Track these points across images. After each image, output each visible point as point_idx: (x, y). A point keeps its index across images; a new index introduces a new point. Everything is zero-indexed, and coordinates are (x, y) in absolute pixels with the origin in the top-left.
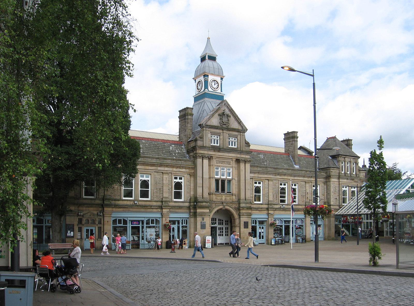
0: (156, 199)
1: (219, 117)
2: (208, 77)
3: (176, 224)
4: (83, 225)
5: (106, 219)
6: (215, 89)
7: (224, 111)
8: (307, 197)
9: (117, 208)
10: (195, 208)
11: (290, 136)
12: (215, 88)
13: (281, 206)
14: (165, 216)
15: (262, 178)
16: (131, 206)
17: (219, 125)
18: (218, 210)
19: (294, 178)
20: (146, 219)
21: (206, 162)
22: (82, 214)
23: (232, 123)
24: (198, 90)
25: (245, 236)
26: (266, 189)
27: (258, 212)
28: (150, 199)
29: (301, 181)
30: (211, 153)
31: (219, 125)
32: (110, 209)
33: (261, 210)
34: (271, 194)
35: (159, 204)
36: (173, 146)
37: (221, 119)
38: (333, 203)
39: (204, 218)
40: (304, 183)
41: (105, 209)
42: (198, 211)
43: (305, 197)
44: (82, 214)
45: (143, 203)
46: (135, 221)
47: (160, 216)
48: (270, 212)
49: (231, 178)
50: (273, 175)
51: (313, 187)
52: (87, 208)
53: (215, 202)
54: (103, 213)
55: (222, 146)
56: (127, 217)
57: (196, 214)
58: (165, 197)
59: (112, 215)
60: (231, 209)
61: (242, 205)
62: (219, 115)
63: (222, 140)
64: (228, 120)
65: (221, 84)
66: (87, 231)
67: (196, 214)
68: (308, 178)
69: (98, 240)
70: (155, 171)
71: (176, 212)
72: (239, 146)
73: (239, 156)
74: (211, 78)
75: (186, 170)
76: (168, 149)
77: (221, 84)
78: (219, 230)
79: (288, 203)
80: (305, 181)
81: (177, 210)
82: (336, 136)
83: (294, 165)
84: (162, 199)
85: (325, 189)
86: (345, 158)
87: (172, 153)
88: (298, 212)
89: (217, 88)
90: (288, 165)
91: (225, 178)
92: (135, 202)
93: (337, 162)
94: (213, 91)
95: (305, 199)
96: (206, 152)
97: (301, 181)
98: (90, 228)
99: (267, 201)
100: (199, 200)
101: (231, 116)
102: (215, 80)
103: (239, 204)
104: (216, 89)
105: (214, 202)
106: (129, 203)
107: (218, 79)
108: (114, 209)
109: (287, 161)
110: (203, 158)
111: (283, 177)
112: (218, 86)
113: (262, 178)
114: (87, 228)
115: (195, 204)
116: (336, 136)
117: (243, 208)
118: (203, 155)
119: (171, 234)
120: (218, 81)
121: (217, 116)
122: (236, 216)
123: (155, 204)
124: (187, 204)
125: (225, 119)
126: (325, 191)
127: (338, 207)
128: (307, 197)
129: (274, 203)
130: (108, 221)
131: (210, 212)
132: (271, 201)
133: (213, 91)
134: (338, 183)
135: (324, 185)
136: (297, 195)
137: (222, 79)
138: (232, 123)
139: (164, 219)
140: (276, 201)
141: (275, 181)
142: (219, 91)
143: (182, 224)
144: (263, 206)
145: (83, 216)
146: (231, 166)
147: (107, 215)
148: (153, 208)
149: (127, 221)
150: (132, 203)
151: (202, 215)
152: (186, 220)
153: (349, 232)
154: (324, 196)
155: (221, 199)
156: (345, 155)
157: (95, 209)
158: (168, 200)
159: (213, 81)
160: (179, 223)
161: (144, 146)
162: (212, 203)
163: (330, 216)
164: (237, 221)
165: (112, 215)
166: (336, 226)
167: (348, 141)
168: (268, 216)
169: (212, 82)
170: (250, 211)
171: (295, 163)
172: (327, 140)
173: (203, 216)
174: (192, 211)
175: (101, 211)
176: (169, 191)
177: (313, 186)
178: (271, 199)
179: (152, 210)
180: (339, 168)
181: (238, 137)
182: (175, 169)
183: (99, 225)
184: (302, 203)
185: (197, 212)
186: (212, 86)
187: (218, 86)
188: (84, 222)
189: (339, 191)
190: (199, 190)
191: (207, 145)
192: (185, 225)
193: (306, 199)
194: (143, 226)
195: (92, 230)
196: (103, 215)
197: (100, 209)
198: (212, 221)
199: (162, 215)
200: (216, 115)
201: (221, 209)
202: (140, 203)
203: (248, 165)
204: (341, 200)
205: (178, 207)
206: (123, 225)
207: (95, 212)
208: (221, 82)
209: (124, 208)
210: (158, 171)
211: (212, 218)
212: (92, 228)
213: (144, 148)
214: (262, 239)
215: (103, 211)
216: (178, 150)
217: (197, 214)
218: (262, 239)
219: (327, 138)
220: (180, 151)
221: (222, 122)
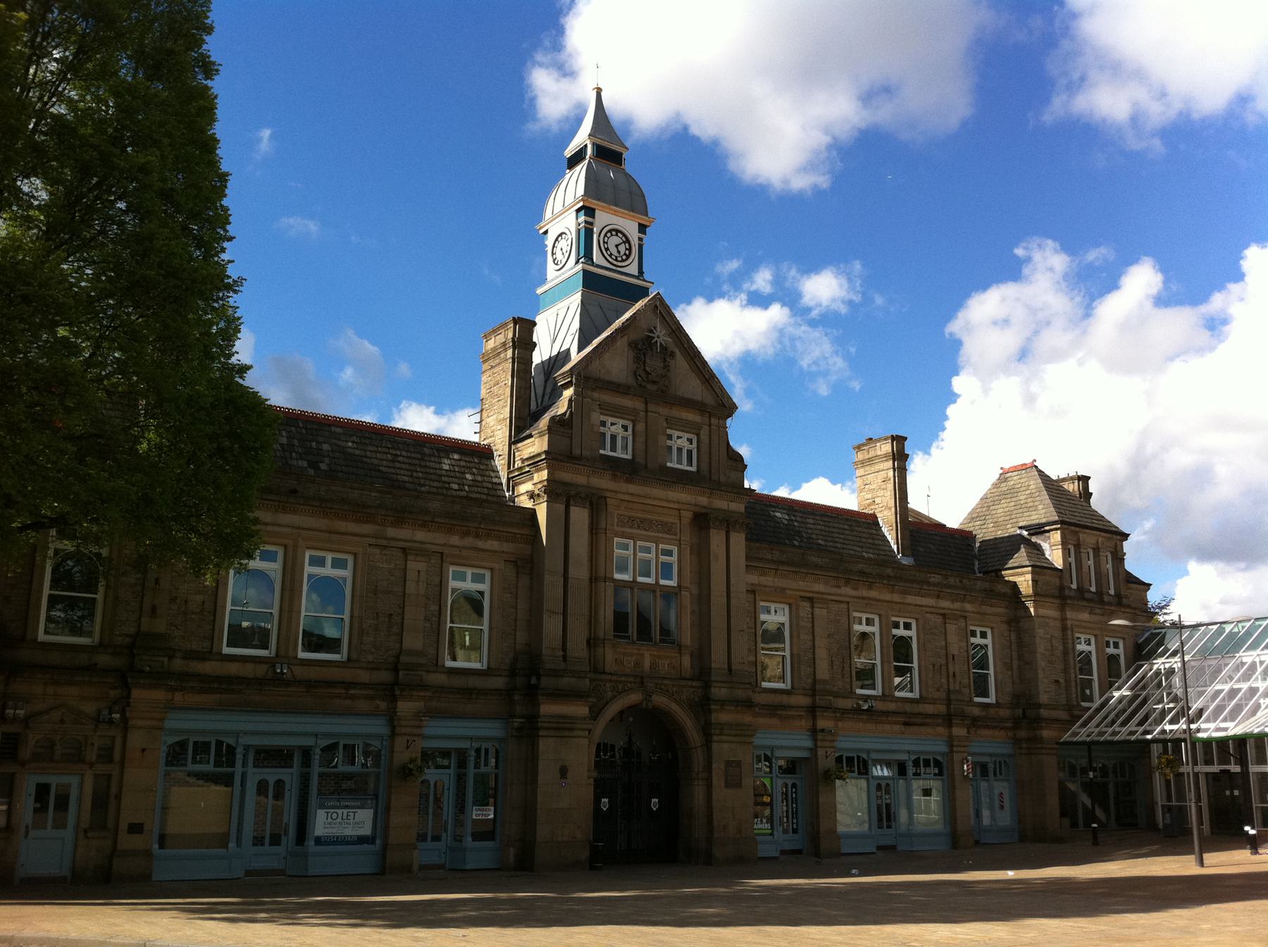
0: (370, 658)
2: (594, 218)
3: (295, 766)
4: (23, 764)
5: (136, 740)
6: (616, 260)
7: (652, 331)
8: (951, 674)
10: (532, 693)
11: (879, 453)
12: (619, 259)
13: (861, 702)
14: (403, 730)
16: (260, 682)
17: (631, 381)
18: (621, 712)
20: (324, 743)
22: (21, 712)
24: (557, 264)
26: (805, 637)
27: (774, 721)
28: (917, 696)
29: (927, 609)
30: (602, 482)
31: (631, 381)
32: (159, 695)
34: (821, 654)
35: (386, 676)
36: (456, 456)
38: (1046, 696)
40: (939, 620)
41: (136, 693)
42: (548, 709)
43: (944, 672)
44: (21, 712)
45: (313, 673)
48: (821, 724)
49: (672, 583)
51: (972, 636)
53: (614, 678)
54: (123, 712)
55: (640, 460)
56: (237, 734)
57: (537, 722)
60: (675, 708)
61: (719, 692)
63: (641, 439)
64: (666, 367)
65: (641, 247)
66: (42, 790)
67: (537, 722)
68: (953, 601)
69: (87, 838)
70: (372, 541)
72: (705, 466)
73: (703, 500)
76: (437, 466)
77: (641, 247)
80: (942, 611)
84: (398, 657)
85: (1014, 647)
87: (449, 483)
88: (923, 729)
89: (624, 257)
90: (877, 552)
91: (654, 582)
92: (278, 666)
93: (1051, 546)
94: (614, 268)
95: (944, 681)
97: (927, 609)
99: (810, 681)
101: (677, 351)
102: (618, 231)
103: (707, 685)
104: (623, 261)
105: (609, 677)
106: (248, 670)
107: (631, 228)
108: (178, 697)
109: (870, 541)
112: (627, 252)
114: (44, 779)
115: (534, 681)
116: (1035, 461)
117: (723, 703)
120: (627, 234)
121: (626, 349)
122: (694, 736)
123: (364, 676)
124: (499, 682)
125: (654, 364)
126: (1015, 654)
127: (1063, 715)
128: (951, 674)
130: (144, 750)
131: (595, 714)
132: (824, 681)
134: (1058, 624)
135: (1010, 631)
137: (642, 228)
139: (400, 742)
141: (835, 607)
142: (633, 269)
143: (477, 766)
145: (26, 722)
146: (676, 540)
147: (140, 723)
148: (353, 698)
149: (235, 749)
150: (261, 670)
151: (564, 726)
153: (1106, 810)
154: (1010, 672)
155: (637, 664)
158: (422, 660)
159: (610, 231)
160: (462, 764)
162: (602, 680)
163: (1039, 746)
164: (698, 758)
165: (168, 724)
166: (1062, 789)
168: (815, 740)
169: (609, 235)
170: (747, 719)
172: (1001, 474)
174: (519, 709)
175: (115, 703)
176: (428, 625)
177: (969, 635)
178: (823, 672)
179: (348, 702)
181: (702, 432)
184: (937, 695)
185: (538, 716)
186: (607, 249)
187: (630, 249)
189: (1065, 653)
190: (551, 626)
191: (586, 453)
193: (951, 680)
194: (465, 775)
195: (280, 784)
196: (125, 720)
197: (113, 693)
198: (598, 755)
199: (393, 728)
201: (632, 708)
202: (299, 672)
203: (739, 541)
204: (1074, 690)
206: (215, 766)
207: (89, 708)
208: (640, 239)
210: (384, 542)
211: (599, 745)
212: (65, 780)
213: (337, 455)
215: (124, 702)
216: (473, 474)
217: (540, 724)
219: (1002, 469)
220: (479, 478)
221: (641, 372)
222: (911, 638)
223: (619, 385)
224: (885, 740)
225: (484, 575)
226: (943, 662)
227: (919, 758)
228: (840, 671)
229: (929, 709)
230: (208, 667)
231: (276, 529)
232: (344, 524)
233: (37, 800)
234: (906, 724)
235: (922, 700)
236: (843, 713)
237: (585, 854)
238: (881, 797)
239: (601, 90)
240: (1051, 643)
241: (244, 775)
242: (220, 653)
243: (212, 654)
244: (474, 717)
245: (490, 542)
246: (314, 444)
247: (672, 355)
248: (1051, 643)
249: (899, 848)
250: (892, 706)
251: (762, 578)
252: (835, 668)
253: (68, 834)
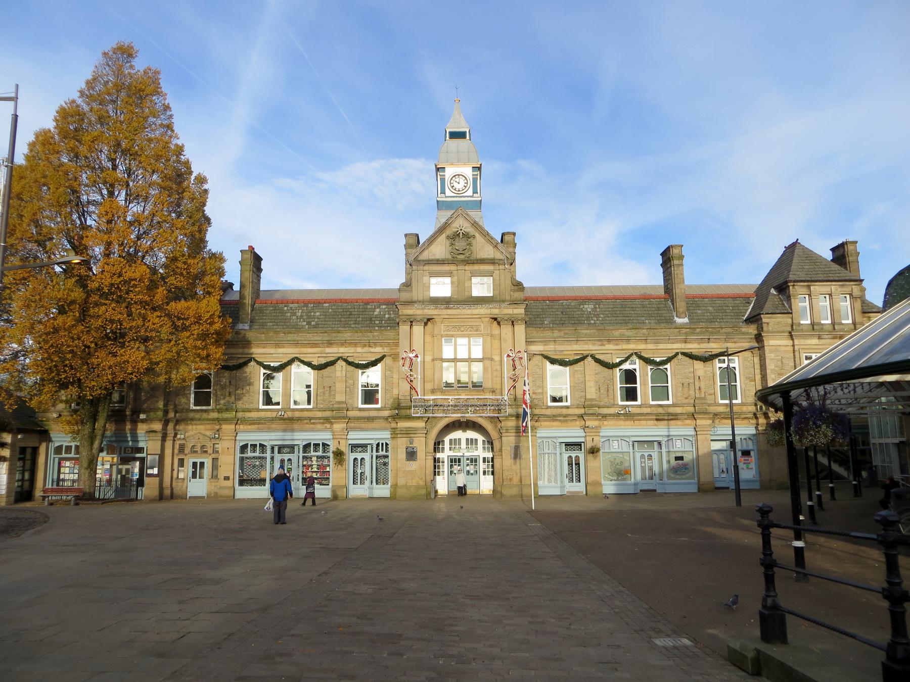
0: (322, 406)
1: (448, 242)
8: (697, 388)
9: (246, 424)
15: (274, 355)
17: (450, 257)
19: (657, 346)
20: (304, 443)
21: (418, 329)
23: (480, 250)
25: (515, 474)
28: (740, 402)
30: (430, 311)
33: (567, 421)
37: (452, 244)
39: (414, 438)
46: (359, 447)
47: (693, 433)
50: (594, 344)
52: (194, 427)
58: (589, 399)
59: (601, 434)
62: (448, 237)
66: (195, 464)
68: (699, 343)
70: (319, 355)
71: (362, 429)
74: (449, 172)
75: (383, 349)
78: (484, 461)
79: (744, 401)
81: (364, 425)
82: (797, 240)
83: (675, 318)
86: (809, 287)
94: (456, 195)
95: (692, 392)
96: (419, 312)
98: (198, 461)
100: (402, 405)
101: (477, 235)
110: (411, 322)
111: (624, 345)
113: (565, 353)
114: (195, 460)
118: (410, 317)
119: (359, 471)
123: (319, 414)
129: (602, 404)
133: (456, 195)
136: (261, 389)
138: (480, 250)
140: (606, 400)
144: (570, 411)
148: (314, 423)
152: (387, 444)
156: (808, 281)
157: (208, 427)
161: (322, 314)
167: (846, 246)
171: (677, 314)
173: (412, 435)
180: (791, 313)
182: (359, 350)
183: (214, 456)
188: (187, 450)
192: (384, 453)
195: (577, 458)
200: (442, 238)
205: (364, 418)
209: (259, 424)
210: (325, 355)
212: (202, 460)
214: (200, 478)
218: (200, 478)
222: (635, 370)
223: (443, 260)
224: (642, 430)
225: (724, 360)
226: (692, 381)
227: (62, 445)
228: (606, 392)
229: (678, 410)
230: (254, 415)
231: (276, 355)
232: (305, 349)
233: (193, 468)
234: (657, 420)
235: (673, 405)
236: (603, 417)
237: (757, 486)
238: (645, 462)
239: (17, 116)
240: (782, 362)
241: (272, 458)
242: (618, 404)
243: (615, 405)
244: (373, 429)
245: (377, 348)
246: (312, 314)
247: (474, 237)
248: (782, 362)
249: (469, 491)
250: (648, 410)
251: (546, 347)
252: (602, 391)
253: (205, 480)
